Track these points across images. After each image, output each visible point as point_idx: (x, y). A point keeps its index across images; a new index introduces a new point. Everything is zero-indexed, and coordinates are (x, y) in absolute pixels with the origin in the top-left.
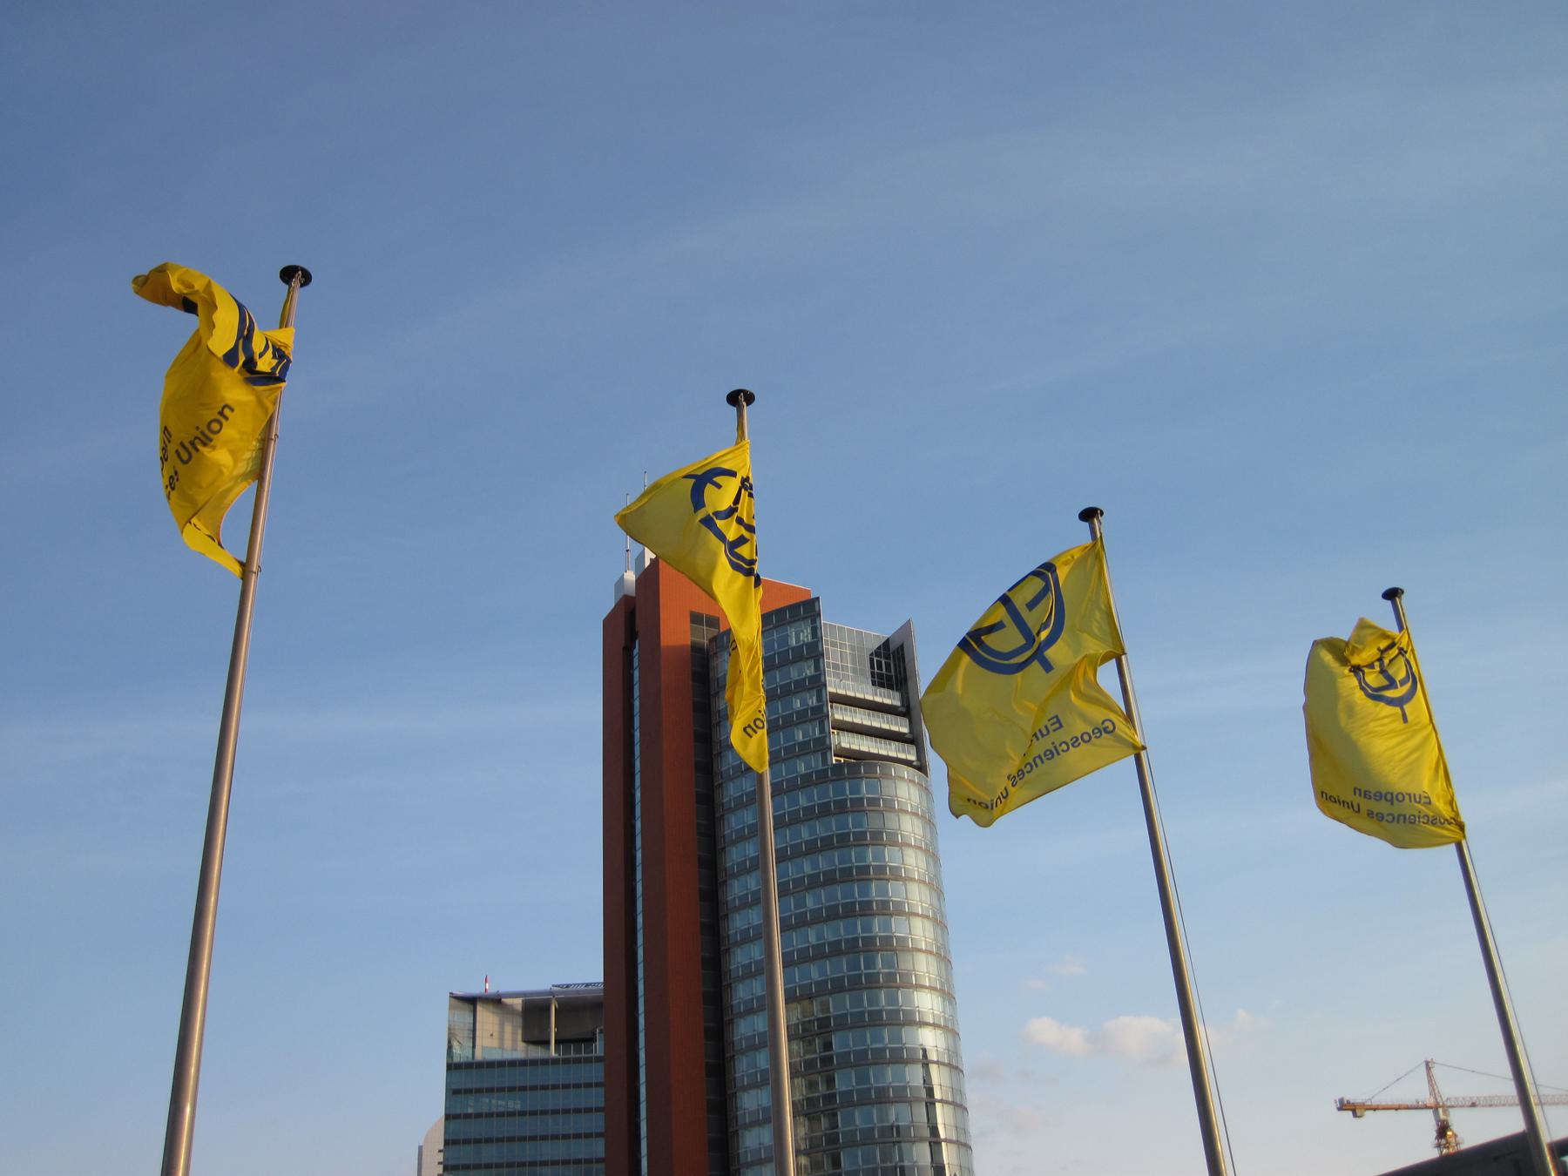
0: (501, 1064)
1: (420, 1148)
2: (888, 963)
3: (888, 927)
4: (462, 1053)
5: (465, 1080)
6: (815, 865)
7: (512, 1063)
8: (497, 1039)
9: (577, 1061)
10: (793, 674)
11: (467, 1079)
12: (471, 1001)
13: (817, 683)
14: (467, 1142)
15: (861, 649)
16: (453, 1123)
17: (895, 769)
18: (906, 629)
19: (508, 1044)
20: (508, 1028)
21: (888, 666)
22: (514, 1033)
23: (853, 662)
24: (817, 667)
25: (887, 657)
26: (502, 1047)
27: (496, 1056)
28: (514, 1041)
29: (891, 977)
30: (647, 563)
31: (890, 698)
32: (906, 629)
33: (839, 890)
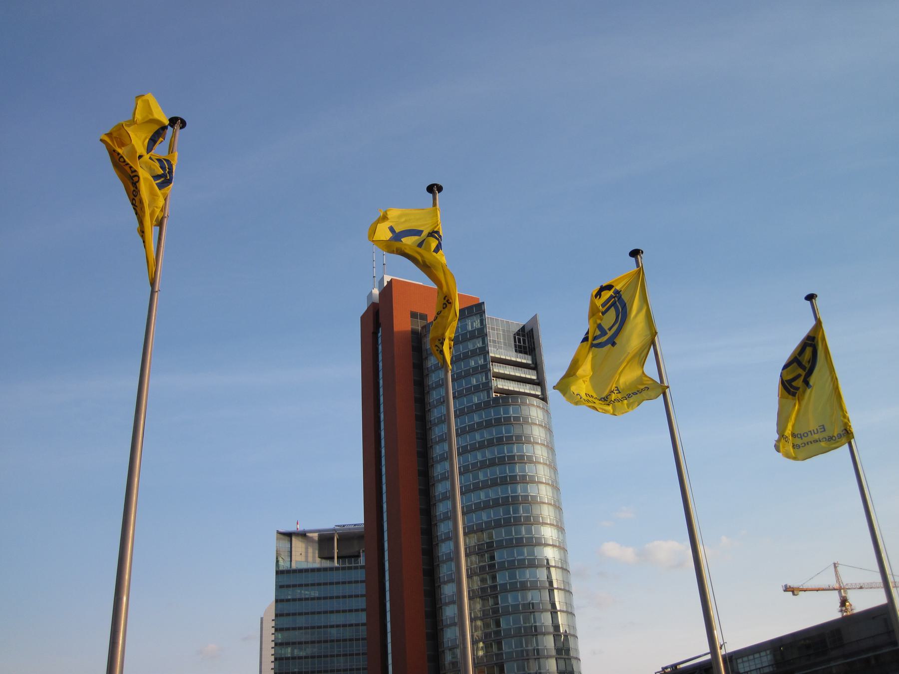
0: (306, 570)
1: (262, 619)
2: (526, 510)
3: (526, 490)
4: (284, 565)
5: (286, 580)
6: (484, 455)
7: (313, 570)
8: (304, 556)
9: (350, 568)
10: (470, 346)
11: (287, 579)
12: (289, 535)
13: (484, 351)
14: (288, 615)
15: (508, 331)
16: (280, 605)
17: (529, 400)
18: (535, 318)
19: (310, 559)
20: (310, 550)
21: (524, 341)
22: (314, 553)
23: (504, 339)
24: (484, 342)
25: (523, 336)
26: (307, 561)
27: (304, 566)
28: (314, 557)
29: (528, 518)
30: (385, 284)
31: (526, 359)
32: (535, 318)
33: (497, 469)
